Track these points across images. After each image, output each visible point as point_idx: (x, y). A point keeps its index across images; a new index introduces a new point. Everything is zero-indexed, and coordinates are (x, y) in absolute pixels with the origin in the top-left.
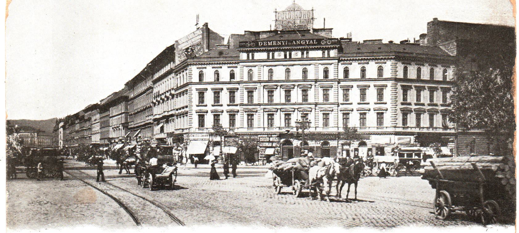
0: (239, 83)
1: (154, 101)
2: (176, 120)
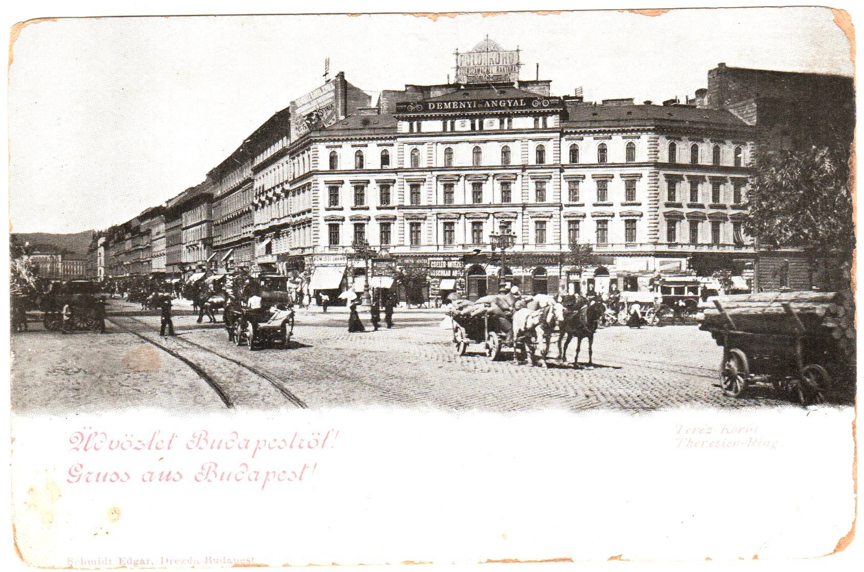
0: (396, 171)
1: (256, 202)
2: (292, 234)
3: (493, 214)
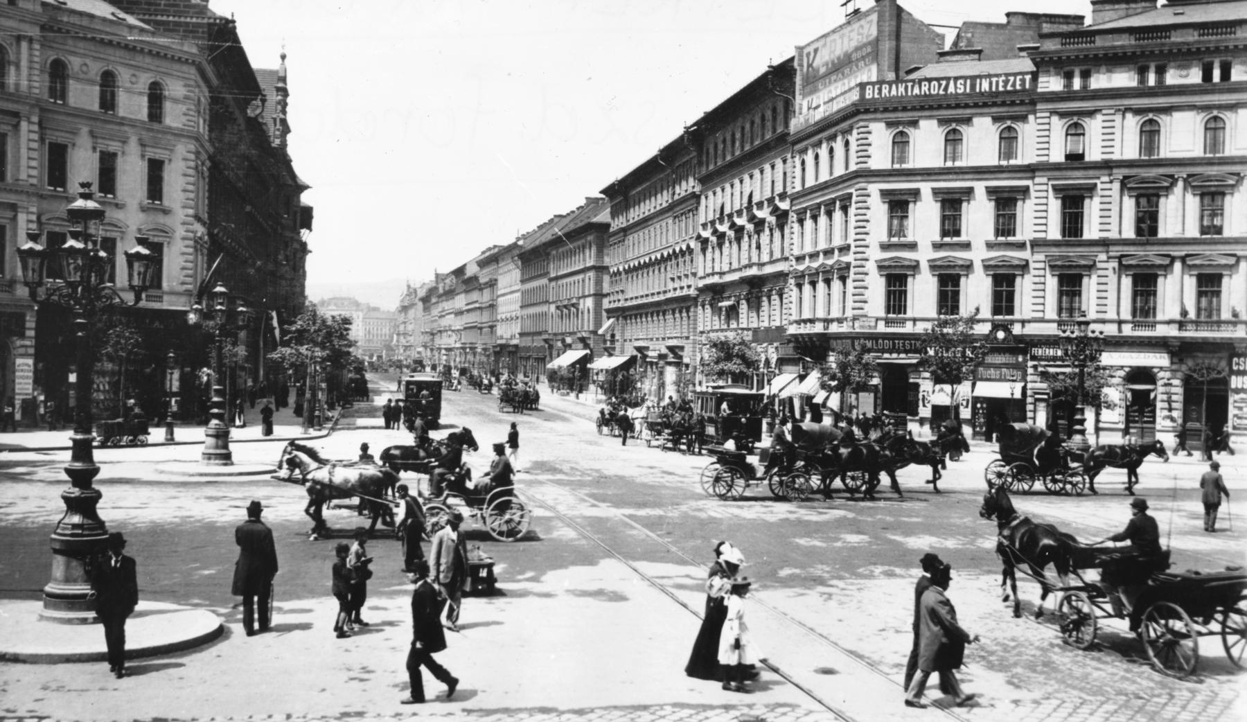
0: (1031, 170)
1: (706, 234)
2: (792, 293)
3: (1183, 259)
